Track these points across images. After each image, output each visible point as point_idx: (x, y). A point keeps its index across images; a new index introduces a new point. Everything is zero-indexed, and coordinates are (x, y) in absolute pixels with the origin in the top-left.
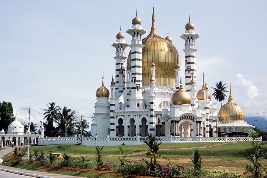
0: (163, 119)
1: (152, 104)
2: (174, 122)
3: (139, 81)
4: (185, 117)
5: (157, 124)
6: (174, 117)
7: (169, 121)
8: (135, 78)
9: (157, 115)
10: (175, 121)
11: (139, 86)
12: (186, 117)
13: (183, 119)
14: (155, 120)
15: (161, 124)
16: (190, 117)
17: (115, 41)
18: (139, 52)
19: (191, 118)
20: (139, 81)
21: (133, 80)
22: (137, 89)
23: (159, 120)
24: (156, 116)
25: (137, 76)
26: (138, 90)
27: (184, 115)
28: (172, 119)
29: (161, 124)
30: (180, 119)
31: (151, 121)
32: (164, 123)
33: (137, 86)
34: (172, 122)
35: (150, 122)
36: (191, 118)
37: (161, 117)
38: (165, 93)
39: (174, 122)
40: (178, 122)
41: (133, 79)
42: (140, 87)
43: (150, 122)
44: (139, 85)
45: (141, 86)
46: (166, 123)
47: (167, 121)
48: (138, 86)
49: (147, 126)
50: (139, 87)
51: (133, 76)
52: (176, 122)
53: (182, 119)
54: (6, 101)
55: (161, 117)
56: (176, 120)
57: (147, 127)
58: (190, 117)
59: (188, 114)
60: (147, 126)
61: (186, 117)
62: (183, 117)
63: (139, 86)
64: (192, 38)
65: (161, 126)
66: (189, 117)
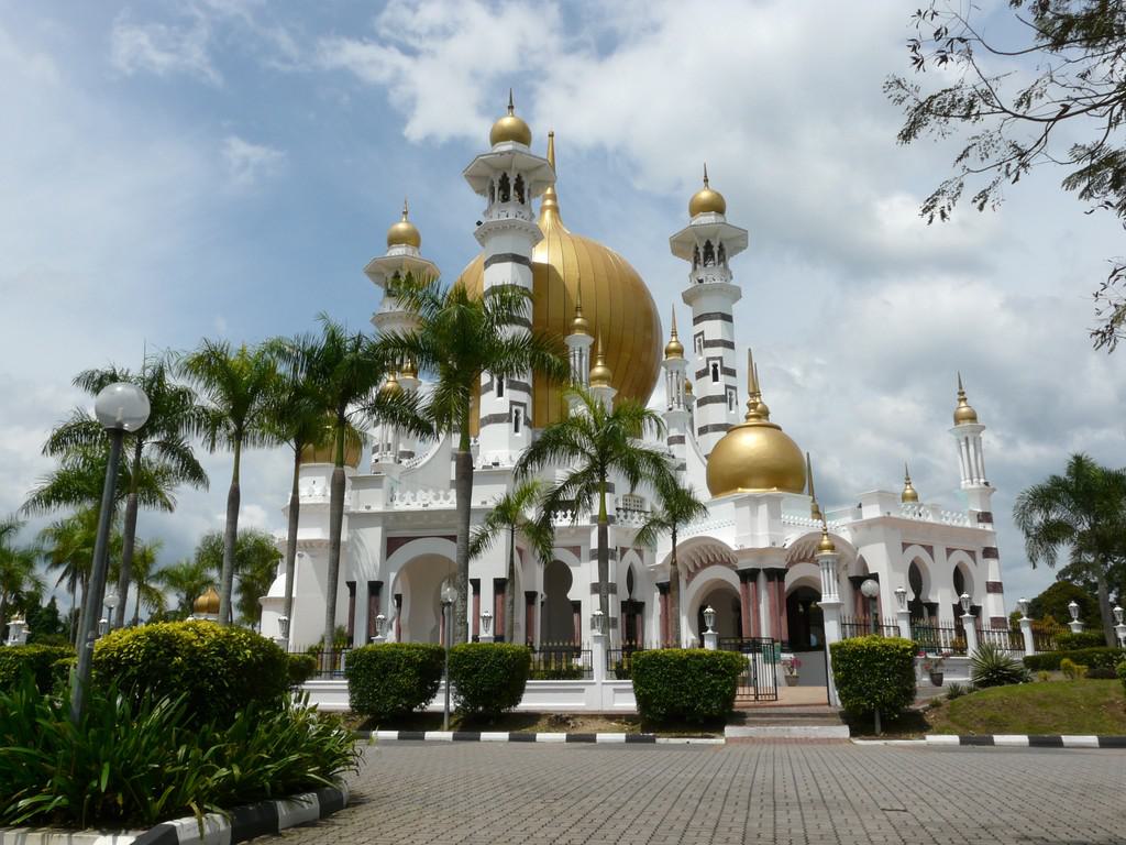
5: (626, 597)
9: (624, 551)
24: (618, 553)
33: (711, 363)
48: (715, 366)
50: (719, 368)
63: (522, 409)
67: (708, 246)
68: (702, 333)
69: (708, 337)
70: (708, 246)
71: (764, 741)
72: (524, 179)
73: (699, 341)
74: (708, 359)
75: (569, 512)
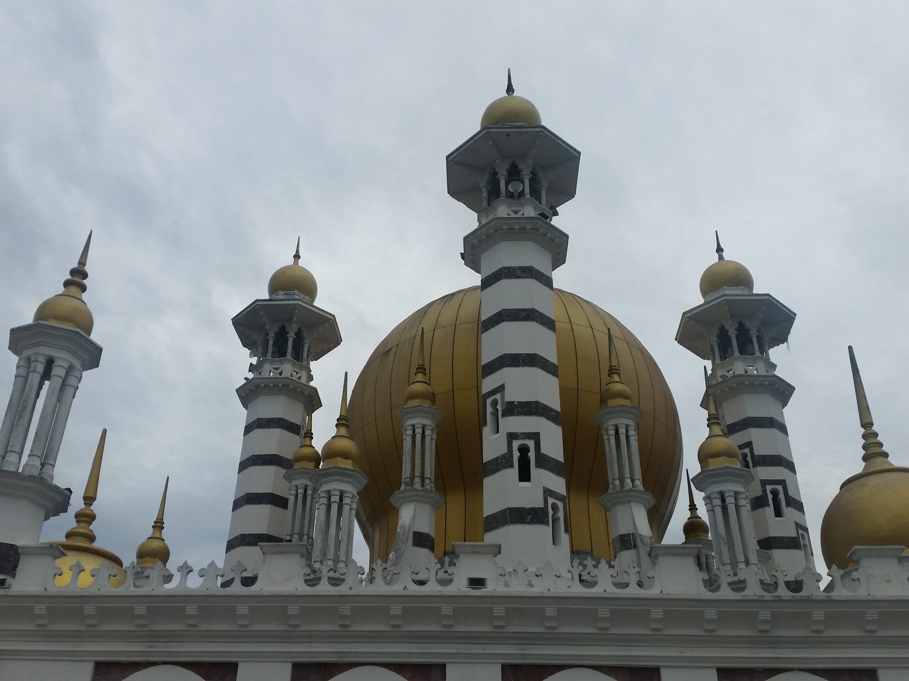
11: (531, 443)
26: (778, 513)
33: (516, 444)
44: (535, 437)
48: (524, 450)
50: (532, 455)
68: (501, 389)
69: (513, 395)
71: (761, 658)
73: (495, 403)
74: (512, 437)
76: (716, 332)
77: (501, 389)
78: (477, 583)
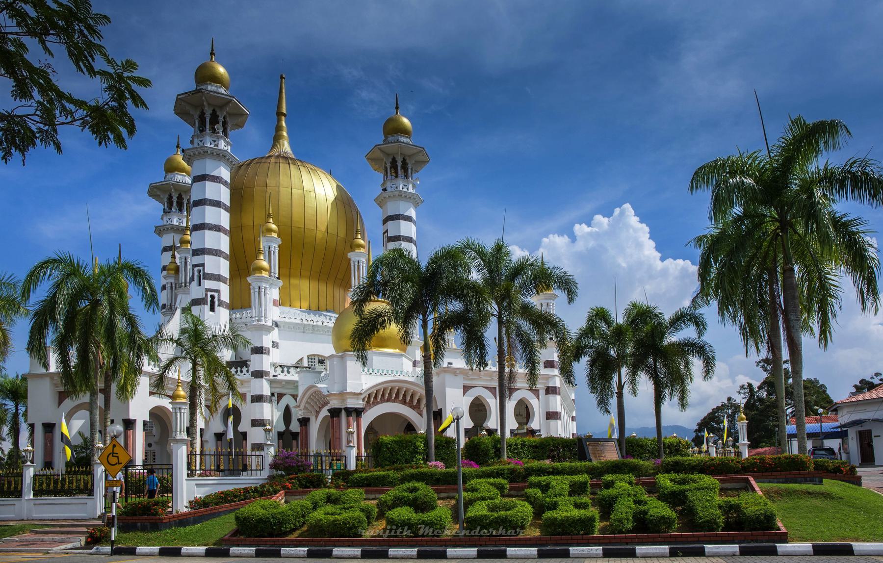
0: (302, 407)
1: (262, 353)
2: (343, 414)
3: (218, 278)
4: (379, 400)
5: (282, 428)
6: (343, 394)
7: (324, 413)
8: (201, 268)
9: (280, 396)
10: (346, 409)
11: (216, 294)
12: (383, 395)
13: (378, 403)
14: (270, 412)
15: (295, 427)
16: (405, 396)
17: (159, 177)
18: (218, 178)
19: (408, 398)
20: (218, 278)
21: (196, 274)
22: (207, 307)
23: (287, 414)
24: (275, 398)
25: (208, 260)
26: (212, 309)
27: (382, 387)
28: (335, 403)
29: (295, 427)
30: (368, 402)
31: (258, 417)
32: (304, 422)
33: (209, 294)
34: (335, 413)
35: (252, 421)
36: (408, 398)
37: (296, 400)
38: (313, 326)
39: (343, 414)
40: (358, 413)
41: (196, 269)
42: (219, 300)
43: (252, 421)
44: (218, 291)
45: (225, 296)
46: (313, 419)
47: (318, 413)
48: (212, 297)
49: (244, 435)
50: (216, 300)
51: (197, 260)
52: (349, 412)
53: (376, 403)
54: (596, 403)
55: (296, 400)
56: (352, 403)
57: (241, 437)
58: (405, 396)
59: (385, 385)
60: (244, 435)
61: (383, 395)
62: (376, 396)
63: (216, 294)
64: (404, 163)
65: (295, 435)
66: (401, 397)
67: (394, 162)
70: (394, 162)
72: (407, 161)
74: (208, 290)
75: (239, 369)
76: (167, 196)
77: (203, 265)
78: (450, 364)
